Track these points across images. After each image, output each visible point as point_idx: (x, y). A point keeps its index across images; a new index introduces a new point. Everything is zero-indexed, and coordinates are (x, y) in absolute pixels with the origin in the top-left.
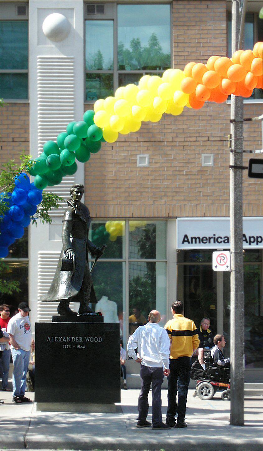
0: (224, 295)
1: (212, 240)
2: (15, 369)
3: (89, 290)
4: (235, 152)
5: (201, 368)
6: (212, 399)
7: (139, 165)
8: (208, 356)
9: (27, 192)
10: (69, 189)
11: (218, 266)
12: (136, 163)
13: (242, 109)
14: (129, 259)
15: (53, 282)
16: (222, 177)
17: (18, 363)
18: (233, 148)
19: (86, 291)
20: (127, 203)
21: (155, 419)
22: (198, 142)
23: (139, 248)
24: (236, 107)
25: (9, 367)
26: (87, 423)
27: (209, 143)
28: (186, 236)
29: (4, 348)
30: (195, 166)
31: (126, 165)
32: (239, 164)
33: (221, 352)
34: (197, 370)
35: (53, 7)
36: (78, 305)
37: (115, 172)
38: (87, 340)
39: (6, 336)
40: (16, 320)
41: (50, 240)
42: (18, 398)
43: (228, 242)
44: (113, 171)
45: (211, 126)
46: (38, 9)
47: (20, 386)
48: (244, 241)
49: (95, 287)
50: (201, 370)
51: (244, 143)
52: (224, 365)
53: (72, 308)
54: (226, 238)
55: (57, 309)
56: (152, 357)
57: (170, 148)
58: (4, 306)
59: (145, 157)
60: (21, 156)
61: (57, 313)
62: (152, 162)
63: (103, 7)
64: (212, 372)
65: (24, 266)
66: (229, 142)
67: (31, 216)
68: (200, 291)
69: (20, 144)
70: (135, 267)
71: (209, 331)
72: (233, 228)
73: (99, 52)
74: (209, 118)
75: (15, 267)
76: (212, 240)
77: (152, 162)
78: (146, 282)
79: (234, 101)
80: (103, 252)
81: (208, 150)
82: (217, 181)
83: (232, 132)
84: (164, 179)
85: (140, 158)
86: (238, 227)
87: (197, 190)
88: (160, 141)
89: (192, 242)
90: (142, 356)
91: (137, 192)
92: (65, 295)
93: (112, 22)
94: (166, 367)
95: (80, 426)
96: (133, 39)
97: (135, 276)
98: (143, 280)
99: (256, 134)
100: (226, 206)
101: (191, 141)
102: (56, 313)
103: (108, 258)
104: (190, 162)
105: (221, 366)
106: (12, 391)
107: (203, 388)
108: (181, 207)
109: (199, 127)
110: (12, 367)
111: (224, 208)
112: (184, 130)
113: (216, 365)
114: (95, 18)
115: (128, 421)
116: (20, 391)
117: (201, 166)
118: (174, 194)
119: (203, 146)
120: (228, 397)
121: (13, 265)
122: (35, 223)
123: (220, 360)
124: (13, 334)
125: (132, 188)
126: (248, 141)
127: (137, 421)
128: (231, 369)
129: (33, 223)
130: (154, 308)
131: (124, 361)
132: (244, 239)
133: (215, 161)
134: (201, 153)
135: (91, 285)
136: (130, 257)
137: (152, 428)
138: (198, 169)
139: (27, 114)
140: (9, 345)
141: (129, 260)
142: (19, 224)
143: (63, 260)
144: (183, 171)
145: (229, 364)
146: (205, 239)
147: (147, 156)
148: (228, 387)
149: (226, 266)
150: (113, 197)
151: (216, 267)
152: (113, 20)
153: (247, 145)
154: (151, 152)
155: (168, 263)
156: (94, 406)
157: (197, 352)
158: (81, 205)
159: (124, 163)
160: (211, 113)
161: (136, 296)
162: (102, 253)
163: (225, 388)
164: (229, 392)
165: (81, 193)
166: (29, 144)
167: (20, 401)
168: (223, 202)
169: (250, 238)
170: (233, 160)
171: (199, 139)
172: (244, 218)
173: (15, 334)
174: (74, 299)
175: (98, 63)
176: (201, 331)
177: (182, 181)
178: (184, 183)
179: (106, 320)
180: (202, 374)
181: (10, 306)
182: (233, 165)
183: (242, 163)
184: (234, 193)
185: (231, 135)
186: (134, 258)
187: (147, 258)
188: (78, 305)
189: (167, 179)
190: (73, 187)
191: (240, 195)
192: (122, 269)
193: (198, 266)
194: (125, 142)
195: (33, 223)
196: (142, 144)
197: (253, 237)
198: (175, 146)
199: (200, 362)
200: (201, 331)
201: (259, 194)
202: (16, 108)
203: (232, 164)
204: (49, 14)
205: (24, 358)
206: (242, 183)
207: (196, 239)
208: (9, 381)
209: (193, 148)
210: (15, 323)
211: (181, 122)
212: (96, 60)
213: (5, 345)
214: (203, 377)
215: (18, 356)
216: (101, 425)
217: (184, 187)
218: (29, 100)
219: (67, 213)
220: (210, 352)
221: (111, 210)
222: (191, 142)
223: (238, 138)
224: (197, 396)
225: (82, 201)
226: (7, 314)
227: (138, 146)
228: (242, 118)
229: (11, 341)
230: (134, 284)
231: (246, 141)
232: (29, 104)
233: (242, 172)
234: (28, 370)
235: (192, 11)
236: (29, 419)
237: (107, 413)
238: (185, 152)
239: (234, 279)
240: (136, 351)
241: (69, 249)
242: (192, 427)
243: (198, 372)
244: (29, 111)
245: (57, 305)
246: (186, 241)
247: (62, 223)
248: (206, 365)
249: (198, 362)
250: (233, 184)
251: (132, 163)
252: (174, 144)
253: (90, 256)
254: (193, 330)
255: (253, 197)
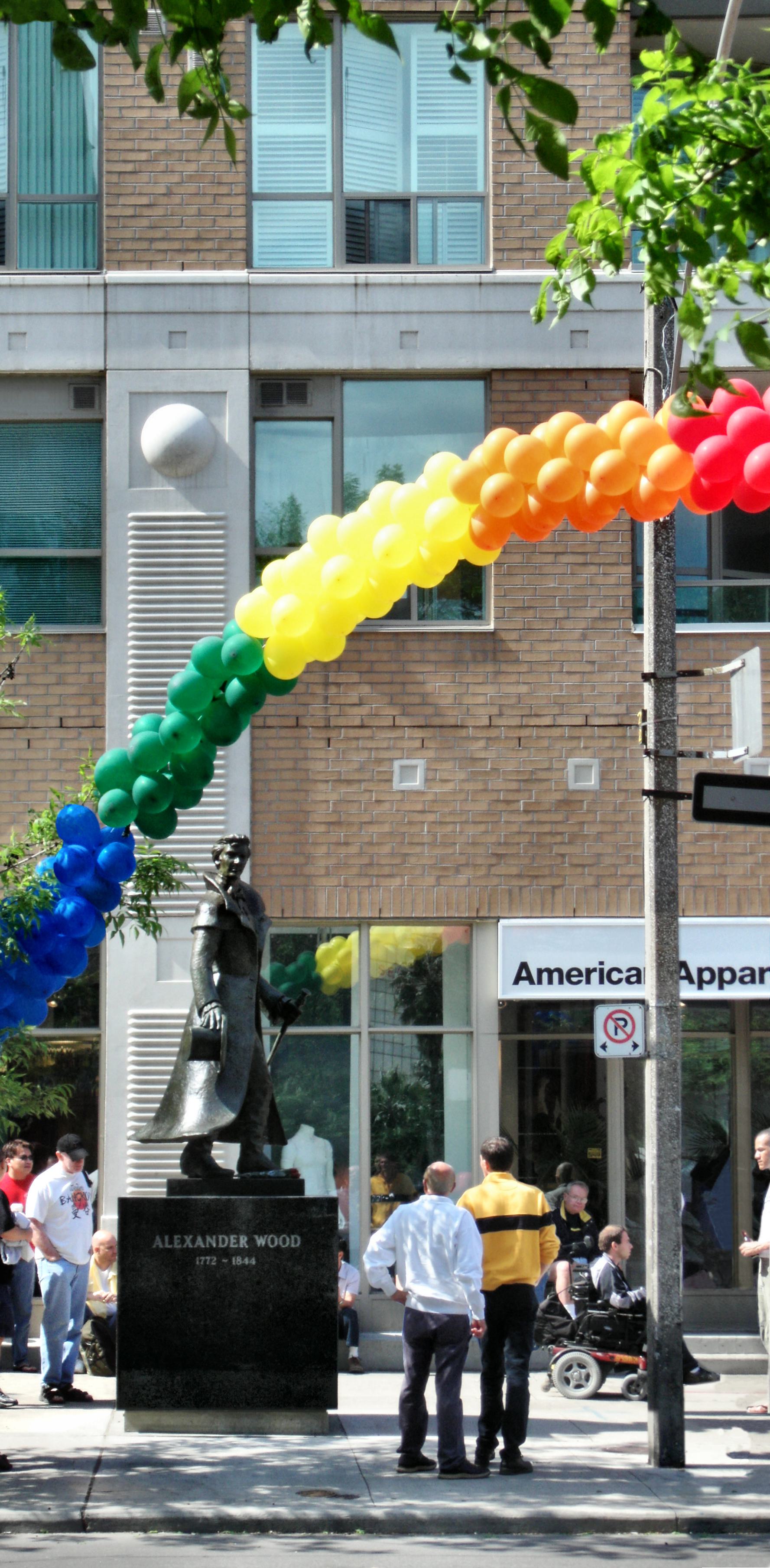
0: (626, 1123)
1: (595, 976)
2: (46, 1313)
3: (265, 1109)
4: (657, 756)
5: (564, 1313)
6: (596, 1396)
7: (397, 785)
8: (583, 1282)
9: (94, 853)
10: (211, 846)
11: (609, 1044)
12: (390, 781)
13: (673, 647)
14: (370, 1026)
15: (168, 1089)
16: (622, 817)
17: (55, 1296)
18: (651, 745)
19: (257, 1113)
20: (366, 882)
21: (446, 1451)
22: (559, 729)
23: (397, 996)
24: (658, 641)
25: (30, 1308)
26: (261, 1461)
27: (587, 731)
28: (524, 966)
29: (17, 1256)
30: (550, 790)
31: (363, 786)
32: (666, 784)
33: (621, 1272)
34: (554, 1320)
35: (171, 388)
36: (235, 1150)
37: (334, 804)
38: (261, 1241)
39: (23, 1225)
40: (51, 1183)
41: (158, 979)
42: (55, 1390)
43: (639, 981)
44: (328, 801)
45: (593, 688)
46: (131, 393)
47: (61, 1357)
48: (682, 978)
49: (278, 1100)
50: (565, 1319)
51: (681, 732)
52: (627, 1306)
53: (220, 1157)
54: (634, 972)
55: (178, 1161)
56: (433, 1287)
57: (482, 744)
58: (17, 1144)
59: (415, 767)
60: (83, 765)
61: (179, 1171)
62: (434, 780)
63: (304, 386)
64: (595, 1325)
65: (88, 1050)
66: (640, 731)
67: (106, 915)
68: (561, 1110)
69: (80, 734)
70: (388, 1048)
71: (586, 1217)
72: (653, 945)
73: (292, 500)
74: (588, 668)
75: (61, 1053)
76: (595, 976)
77: (434, 780)
78: (418, 1085)
79: (652, 627)
80: (301, 1009)
81: (585, 748)
82: (608, 828)
83: (648, 703)
84: (466, 822)
85: (402, 767)
86: (667, 943)
87: (556, 849)
88: (457, 726)
89: (540, 982)
90: (409, 1284)
91: (392, 855)
92: (200, 1125)
93: (327, 425)
94: (477, 1315)
95: (243, 1469)
96: (384, 466)
97: (389, 1070)
98: (411, 1081)
99: (715, 710)
100: (632, 892)
101: (539, 726)
102: (177, 1172)
103: (313, 1024)
104: (536, 780)
105: (621, 1310)
106: (37, 1370)
107: (569, 1368)
108: (510, 892)
109: (561, 691)
110: (38, 1308)
111: (627, 896)
112: (519, 696)
113: (606, 1305)
114: (284, 415)
115: (369, 1457)
116: (60, 1371)
117: (567, 790)
118: (493, 861)
119: (572, 738)
120: (642, 1391)
121: (58, 1046)
122: (118, 935)
123: (618, 1293)
124: (41, 1220)
125: (378, 844)
126: (691, 726)
127: (398, 1455)
128: (648, 1318)
129: (113, 934)
130: (440, 1157)
131: (353, 1296)
132: (683, 973)
133: (603, 777)
134: (567, 758)
135: (268, 1097)
136: (373, 1022)
137: (437, 1475)
138: (558, 796)
139: (99, 657)
140: (30, 1248)
141: (372, 1029)
142: (78, 943)
143: (196, 1033)
144: (518, 801)
145: (641, 1306)
146: (574, 973)
147: (420, 764)
148: (641, 1366)
149: (630, 1043)
150: (327, 868)
151: (604, 1047)
152: (331, 419)
153: (689, 737)
154: (431, 754)
155: (475, 1035)
156: (281, 1419)
157: (553, 1273)
158: (241, 887)
159: (359, 781)
160: (594, 657)
161: (392, 1124)
162: (297, 1013)
163: (633, 1368)
164: (642, 1379)
165: (243, 857)
166: (104, 731)
167: (61, 1398)
168: (624, 881)
169: (700, 971)
170: (652, 775)
171: (561, 721)
172: (682, 920)
173: (46, 1220)
174: (226, 1134)
175: (288, 528)
176: (563, 1214)
177: (515, 828)
178: (519, 833)
179: (312, 1190)
180: (567, 1330)
181: (34, 1144)
182: (653, 788)
183: (676, 784)
184: (656, 860)
185: (644, 712)
186: (385, 1023)
187: (419, 1023)
188: (235, 1150)
189: (474, 823)
190: (221, 841)
191: (671, 865)
192: (349, 1053)
193: (557, 1044)
194: (362, 727)
195: (113, 934)
196: (407, 732)
197: (710, 970)
198: (497, 738)
199: (562, 1298)
200: (563, 1214)
201: (725, 863)
202: (70, 646)
203: (648, 784)
204: (157, 406)
205: (71, 1284)
206: (675, 836)
207: (550, 974)
208: (30, 1345)
209: (546, 743)
210: (47, 1191)
211: (513, 678)
212: (282, 521)
213: (20, 1248)
214: (571, 1337)
215: (54, 1280)
216: (299, 1466)
217: (518, 844)
218: (104, 626)
219: (205, 908)
220: (589, 1272)
221: (322, 898)
222: (540, 730)
223: (664, 719)
224: (553, 1389)
225: (245, 877)
226: (27, 1166)
227: (395, 738)
228: (673, 668)
229: (36, 1237)
230: (384, 1093)
231: (683, 726)
232: (104, 635)
233: (675, 806)
234: (88, 1314)
235: (543, 396)
236: (96, 1454)
237: (315, 1434)
238: (524, 754)
239: (654, 1074)
240: (392, 1271)
241: (210, 1003)
242: (545, 1471)
243: (556, 1324)
244: (104, 652)
245: (178, 1150)
246: (524, 979)
247: (192, 936)
248: (579, 1307)
249: (556, 1298)
250: (652, 837)
251: (381, 781)
252: (493, 733)
253: (265, 1021)
254: (539, 1214)
255: (706, 871)
